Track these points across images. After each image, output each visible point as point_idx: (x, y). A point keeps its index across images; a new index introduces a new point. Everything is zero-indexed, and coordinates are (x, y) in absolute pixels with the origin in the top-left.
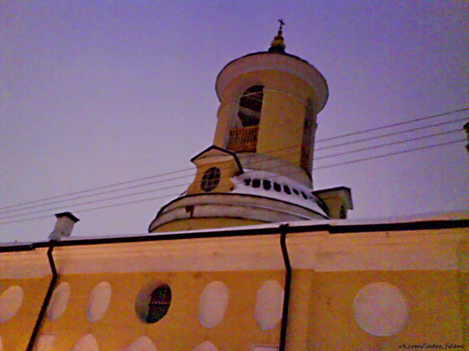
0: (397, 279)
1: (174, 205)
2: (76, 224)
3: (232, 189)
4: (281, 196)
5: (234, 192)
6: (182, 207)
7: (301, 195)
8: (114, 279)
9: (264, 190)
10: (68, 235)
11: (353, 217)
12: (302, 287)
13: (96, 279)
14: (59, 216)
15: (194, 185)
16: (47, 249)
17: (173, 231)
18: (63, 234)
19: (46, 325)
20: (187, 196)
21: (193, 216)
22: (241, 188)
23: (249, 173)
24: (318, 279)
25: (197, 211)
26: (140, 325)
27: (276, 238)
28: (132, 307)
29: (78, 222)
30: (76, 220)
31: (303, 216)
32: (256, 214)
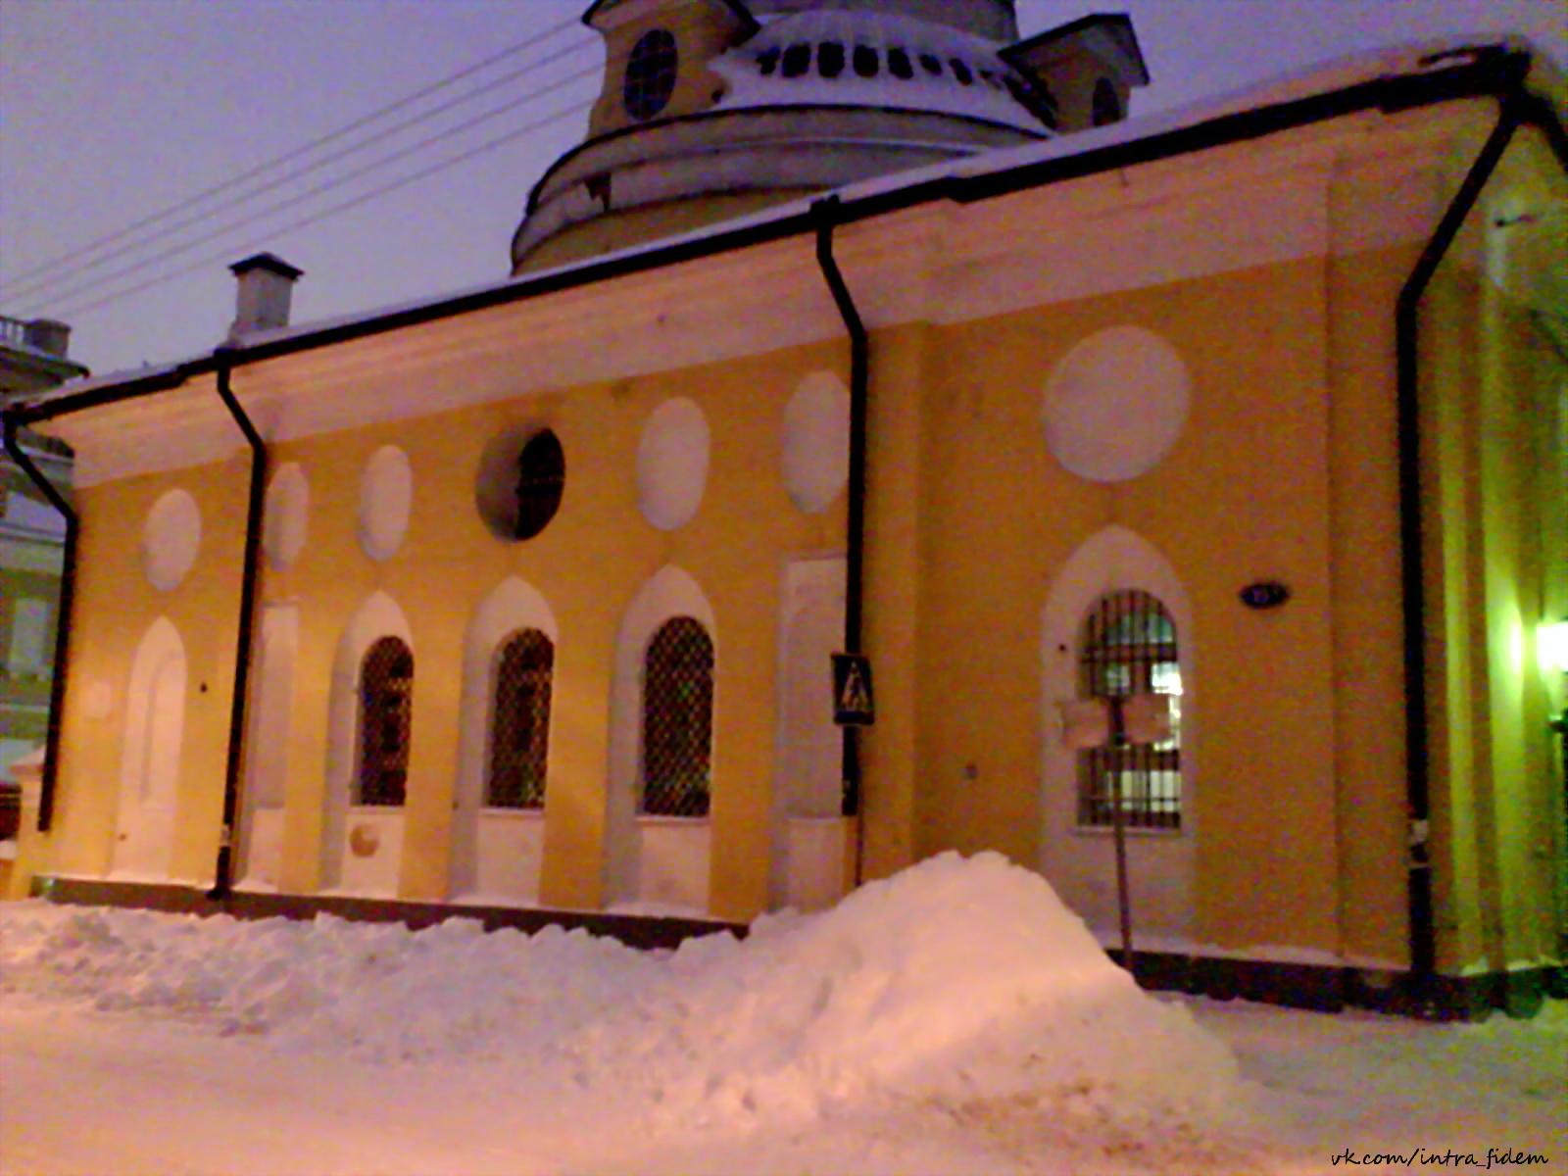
0: (1156, 308)
1: (555, 182)
2: (297, 288)
3: (717, 96)
4: (882, 91)
5: (727, 103)
6: (576, 183)
7: (949, 71)
8: (416, 435)
9: (819, 80)
10: (282, 323)
11: (1148, 110)
12: (899, 375)
13: (370, 439)
14: (240, 269)
15: (602, 108)
16: (212, 377)
17: (651, 238)
18: (262, 322)
19: (270, 582)
20: (590, 143)
21: (613, 205)
22: (747, 86)
23: (781, 29)
24: (943, 345)
25: (622, 189)
26: (500, 550)
27: (801, 250)
28: (468, 500)
29: (302, 279)
30: (291, 274)
31: (948, 146)
32: (795, 168)
